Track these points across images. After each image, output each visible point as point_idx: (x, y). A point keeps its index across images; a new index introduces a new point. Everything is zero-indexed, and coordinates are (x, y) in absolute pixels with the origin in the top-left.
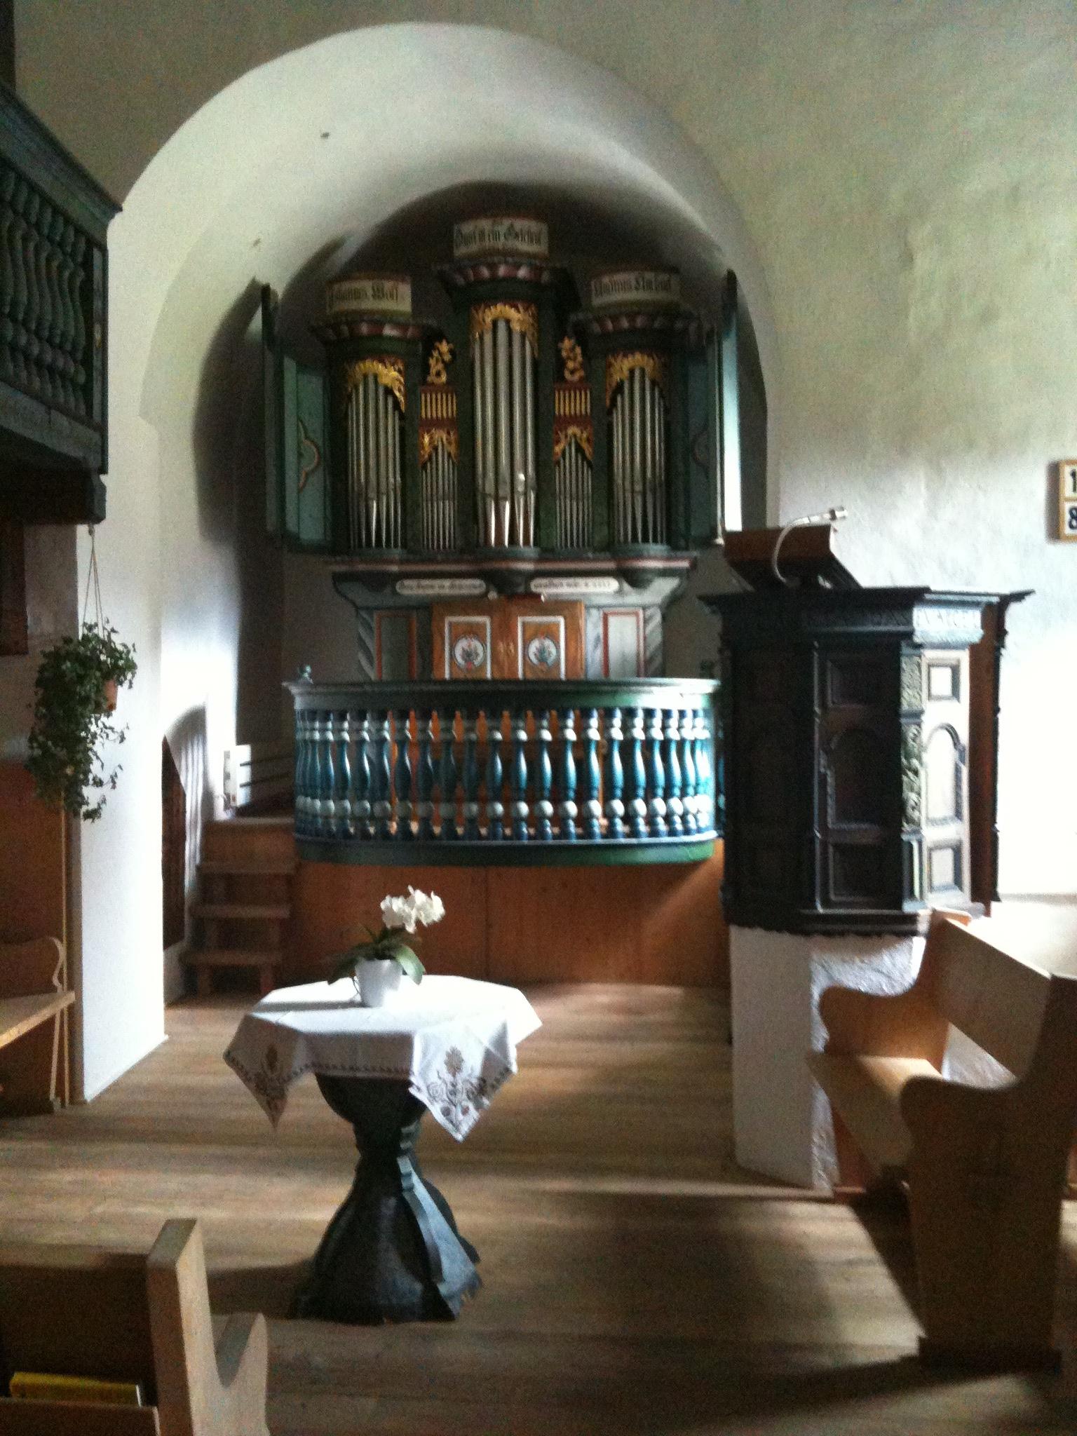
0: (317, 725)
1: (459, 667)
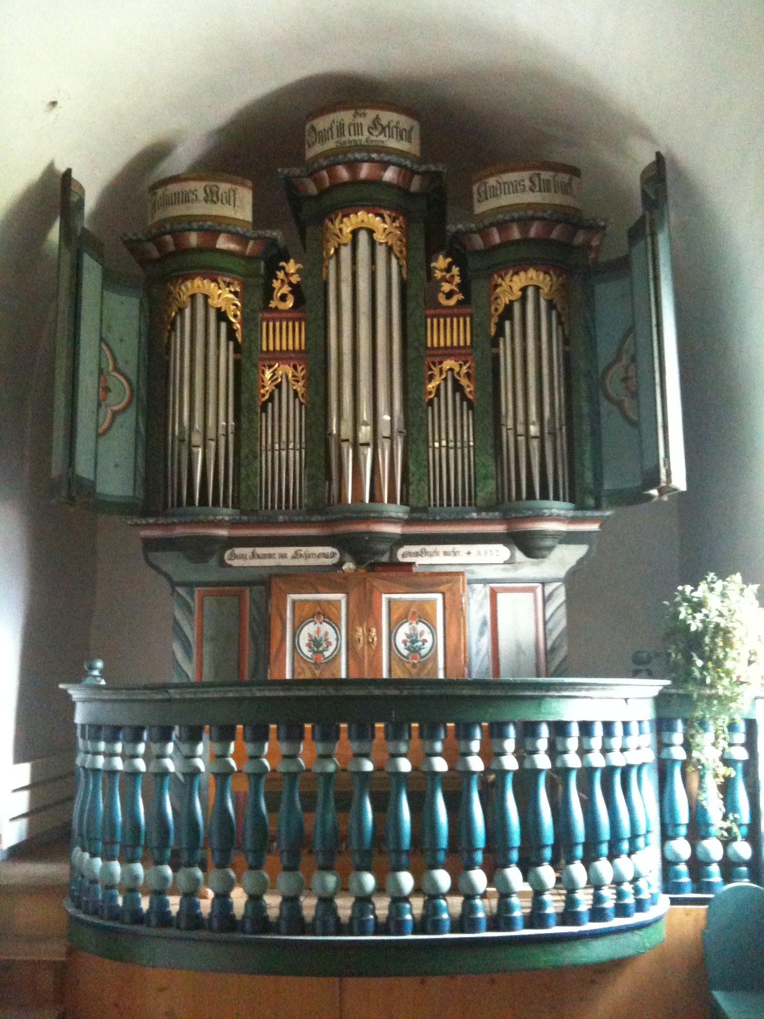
0: (102, 746)
1: (305, 661)
